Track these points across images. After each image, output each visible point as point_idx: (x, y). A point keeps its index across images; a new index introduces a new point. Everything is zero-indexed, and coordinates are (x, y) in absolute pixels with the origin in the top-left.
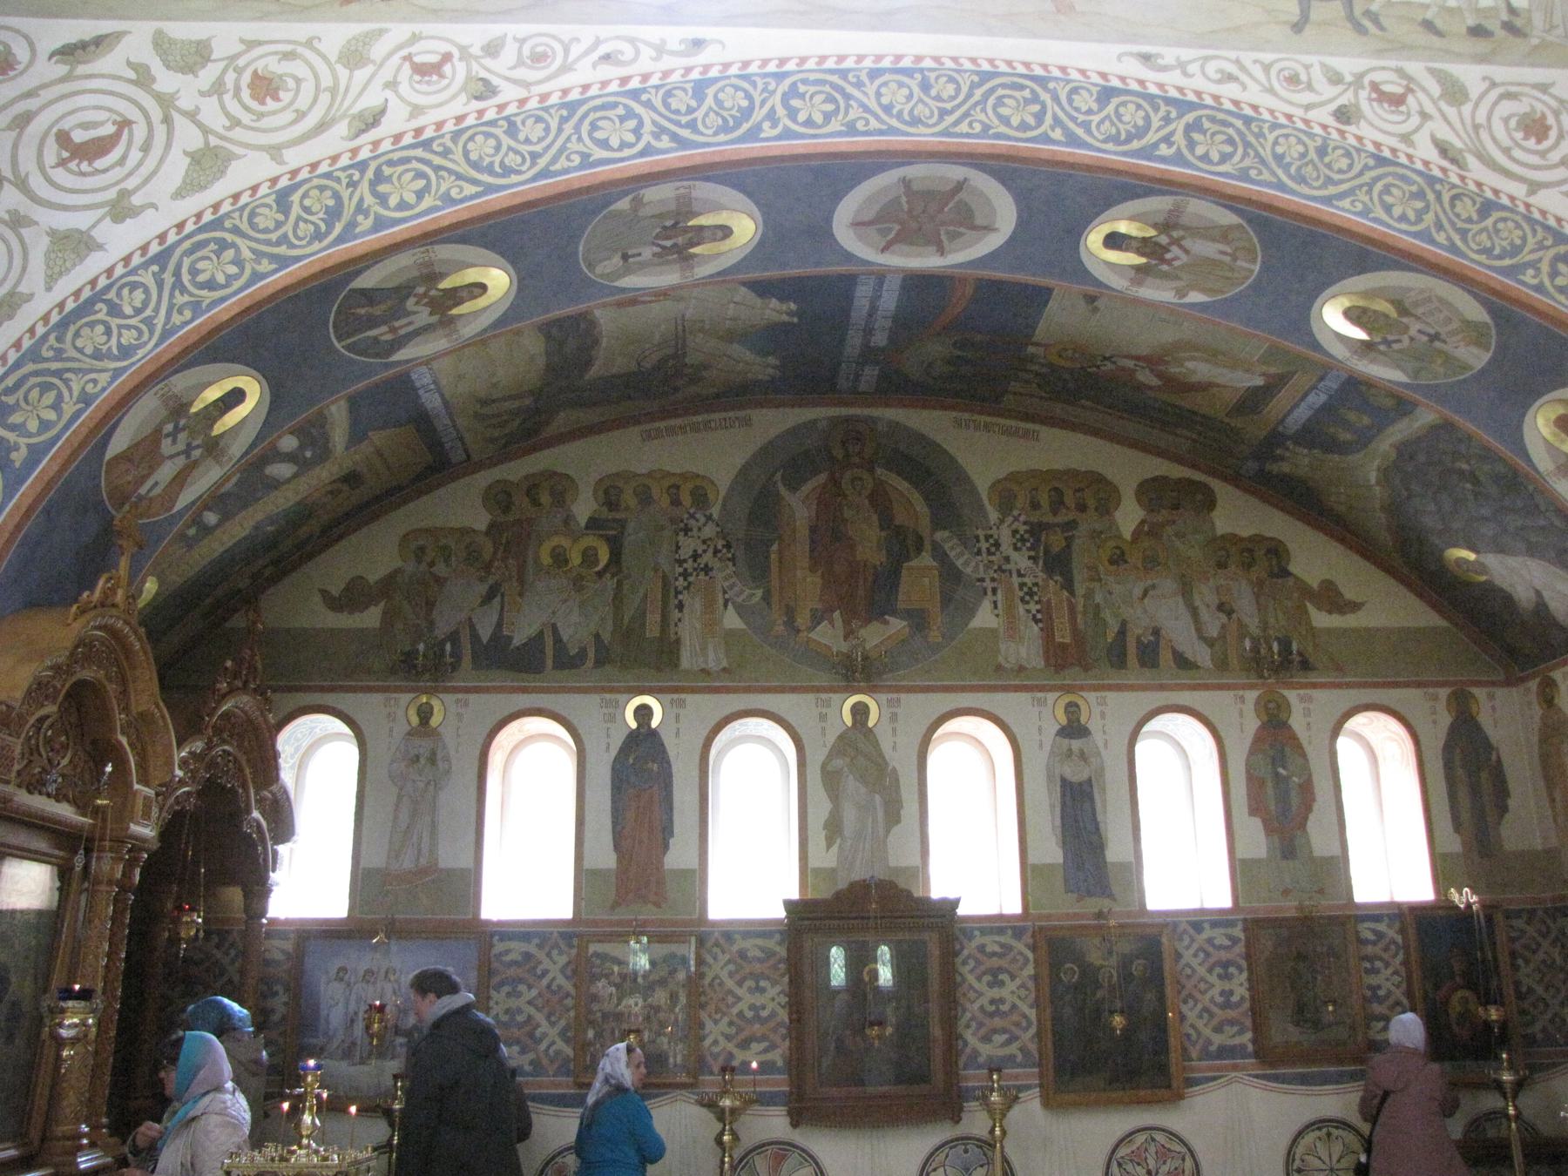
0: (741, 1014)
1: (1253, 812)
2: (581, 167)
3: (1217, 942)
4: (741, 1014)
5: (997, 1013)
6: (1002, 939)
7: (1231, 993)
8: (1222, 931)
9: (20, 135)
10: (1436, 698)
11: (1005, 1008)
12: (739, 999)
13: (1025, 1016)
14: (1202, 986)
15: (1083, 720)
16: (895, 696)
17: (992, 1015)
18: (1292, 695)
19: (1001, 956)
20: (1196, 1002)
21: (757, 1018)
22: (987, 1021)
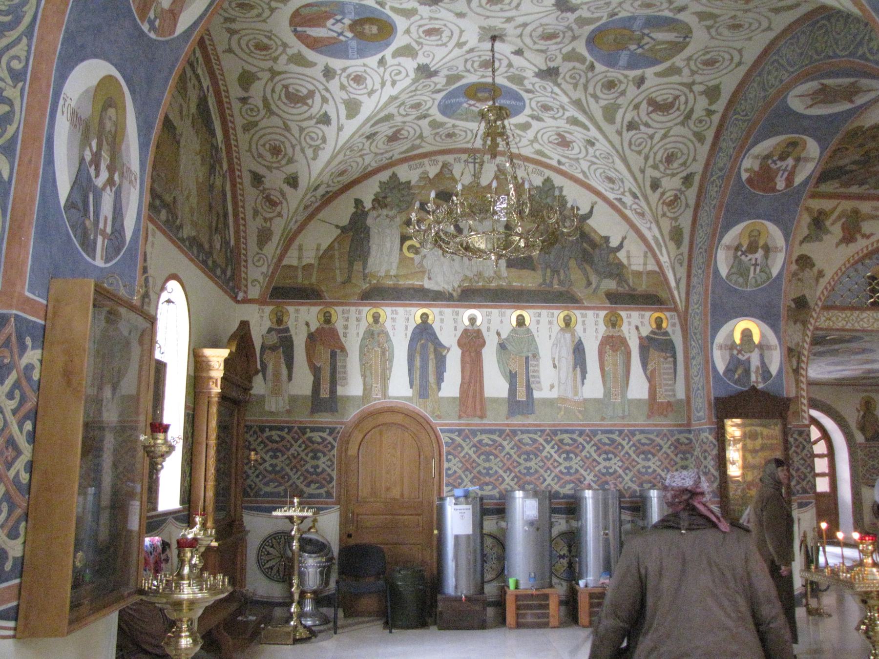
0: (639, 471)
1: (160, 368)
2: (811, 63)
3: (565, 441)
4: (599, 471)
5: (488, 474)
6: (492, 437)
7: (276, 465)
8: (569, 435)
9: (459, 40)
10: (598, 316)
11: (532, 471)
12: (638, 463)
13: (714, 476)
14: (634, 463)
15: (430, 321)
16: (539, 311)
17: (311, 474)
18: (623, 314)
19: (609, 445)
20: (552, 471)
21: (647, 473)
22: (267, 474)
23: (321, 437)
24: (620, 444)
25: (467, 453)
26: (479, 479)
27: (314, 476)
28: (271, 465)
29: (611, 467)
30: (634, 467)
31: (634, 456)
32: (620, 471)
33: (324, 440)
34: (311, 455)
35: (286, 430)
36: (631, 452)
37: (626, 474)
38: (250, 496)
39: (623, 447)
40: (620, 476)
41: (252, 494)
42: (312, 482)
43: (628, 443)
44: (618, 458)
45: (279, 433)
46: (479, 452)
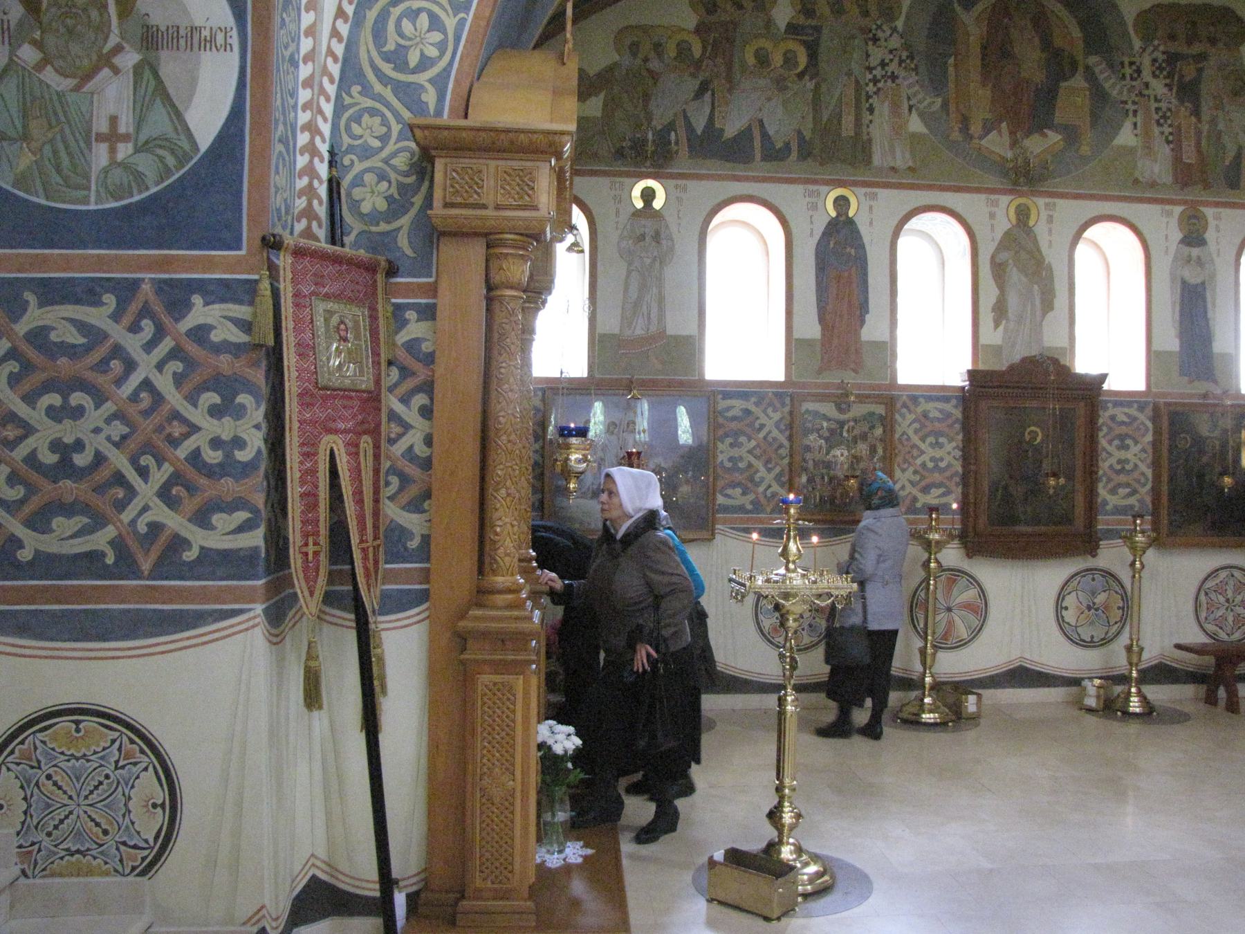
17: (1118, 472)
23: (82, 327)
24: (117, 351)
25: (147, 384)
26: (191, 489)
27: (936, 475)
28: (740, 445)
29: (942, 459)
30: (174, 442)
31: (174, 398)
32: (119, 461)
33: (95, 336)
34: (1116, 442)
35: (110, 300)
36: (164, 383)
37: (143, 473)
38: (137, 575)
39: (130, 366)
40: (119, 479)
41: (146, 566)
42: (1119, 485)
43: (149, 346)
44: (1139, 447)
45: (1126, 410)
46: (196, 378)
